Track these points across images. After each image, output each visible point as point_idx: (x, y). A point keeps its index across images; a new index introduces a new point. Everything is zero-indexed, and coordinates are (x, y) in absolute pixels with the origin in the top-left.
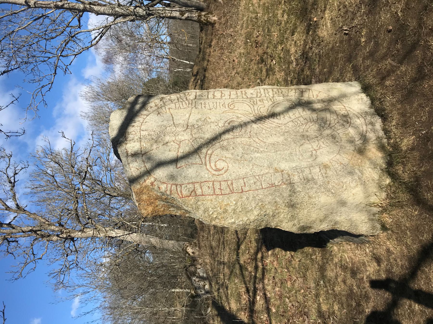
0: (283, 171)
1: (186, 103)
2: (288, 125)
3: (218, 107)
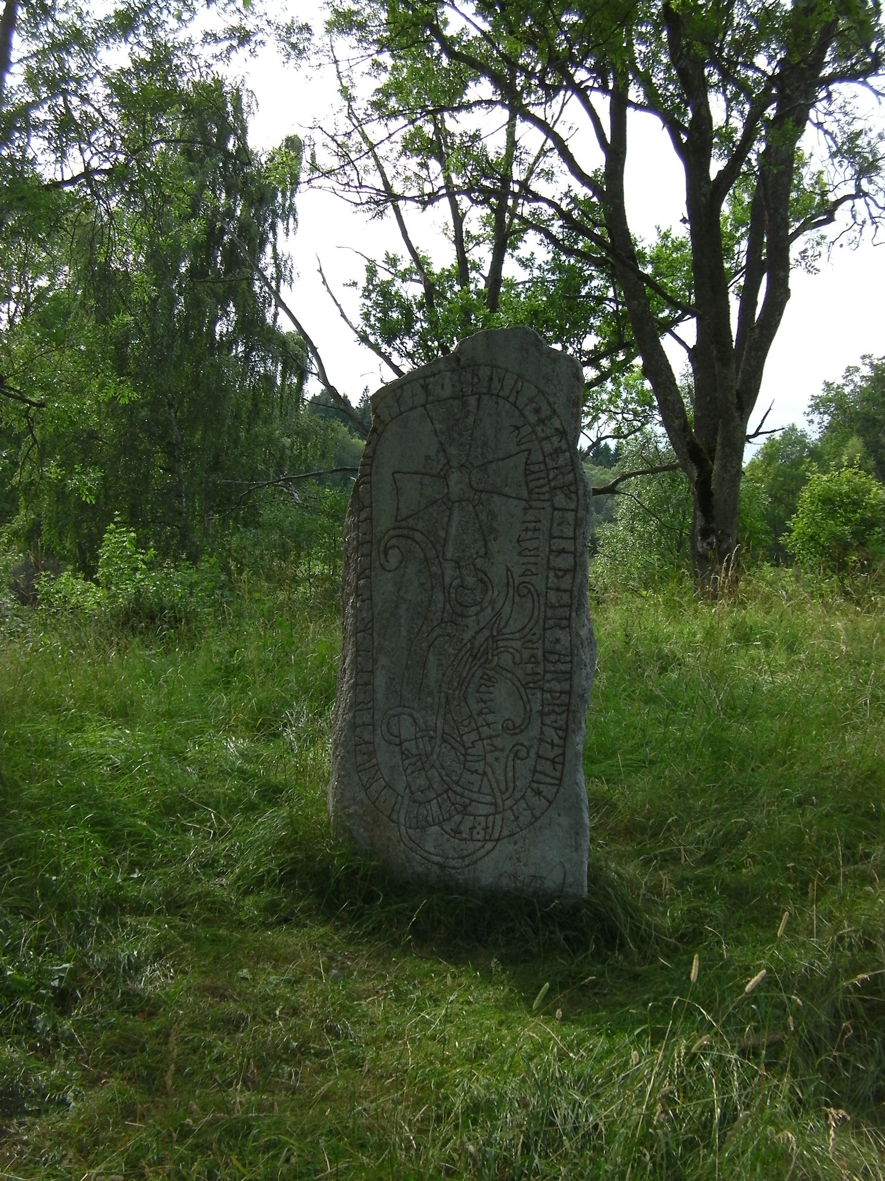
1: (543, 486)
3: (525, 560)
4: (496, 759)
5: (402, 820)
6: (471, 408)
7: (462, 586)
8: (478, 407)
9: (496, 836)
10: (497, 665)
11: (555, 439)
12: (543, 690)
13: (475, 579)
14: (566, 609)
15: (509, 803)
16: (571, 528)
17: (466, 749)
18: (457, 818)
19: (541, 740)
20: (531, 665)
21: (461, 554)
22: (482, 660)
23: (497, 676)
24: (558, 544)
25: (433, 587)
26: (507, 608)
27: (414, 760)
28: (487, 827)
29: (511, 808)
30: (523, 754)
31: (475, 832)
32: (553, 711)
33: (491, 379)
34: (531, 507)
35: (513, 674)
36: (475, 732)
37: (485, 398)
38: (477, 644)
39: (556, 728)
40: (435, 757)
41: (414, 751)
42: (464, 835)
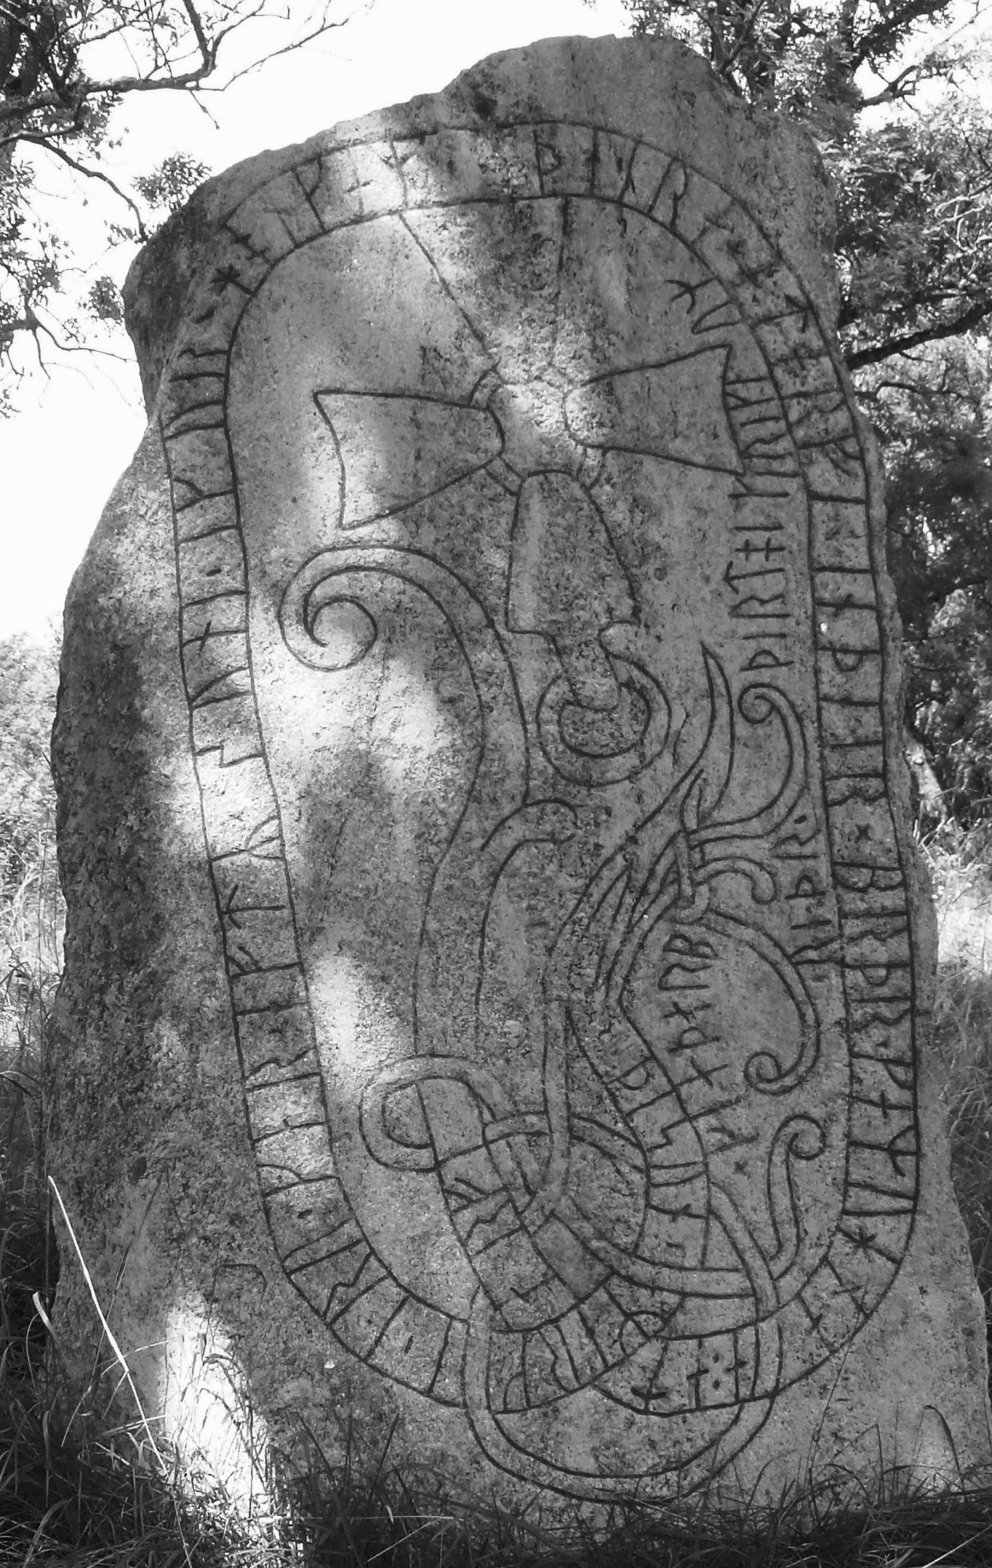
0: (303, 972)
1: (776, 438)
3: (754, 627)
4: (740, 1168)
5: (477, 1392)
6: (545, 230)
7: (576, 700)
8: (567, 228)
9: (769, 1383)
10: (709, 909)
11: (790, 323)
12: (842, 964)
13: (609, 682)
14: (872, 750)
15: (789, 1284)
16: (861, 544)
17: (646, 1151)
18: (648, 1354)
19: (853, 1099)
20: (803, 902)
21: (560, 616)
22: (665, 899)
23: (712, 940)
24: (834, 586)
25: (484, 708)
26: (717, 753)
27: (490, 1205)
28: (740, 1364)
29: (798, 1296)
30: (810, 1142)
31: (706, 1383)
32: (876, 1017)
33: (593, 159)
34: (750, 491)
36: (669, 1102)
37: (586, 209)
38: (644, 855)
39: (886, 1062)
40: (555, 1188)
41: (489, 1181)
42: (676, 1400)
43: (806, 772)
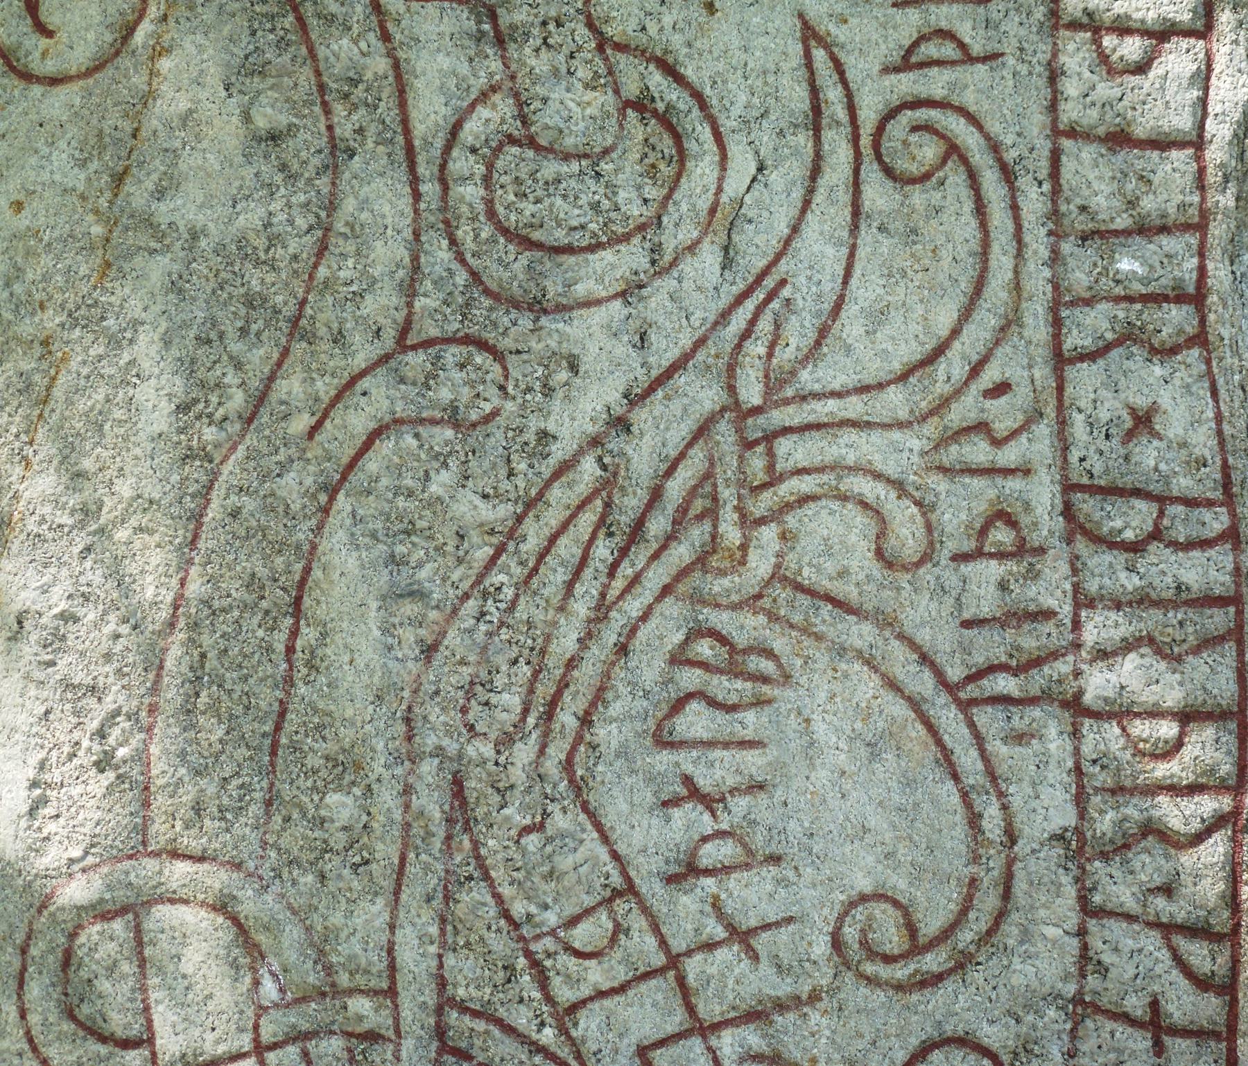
2: (560, 821)
10: (778, 576)
13: (603, 100)
19: (1082, 1008)
20: (993, 570)
22: (681, 553)
25: (338, 152)
26: (820, 247)
35: (886, 621)
36: (658, 990)
39: (1167, 929)
43: (1017, 286)
